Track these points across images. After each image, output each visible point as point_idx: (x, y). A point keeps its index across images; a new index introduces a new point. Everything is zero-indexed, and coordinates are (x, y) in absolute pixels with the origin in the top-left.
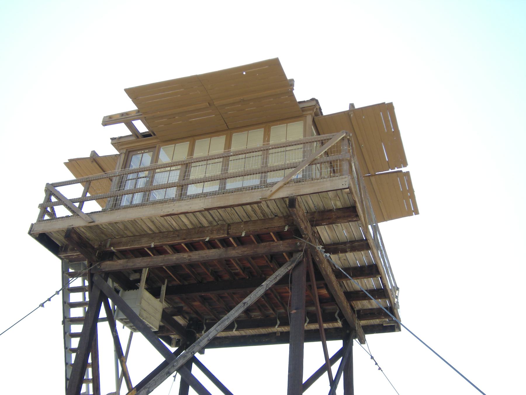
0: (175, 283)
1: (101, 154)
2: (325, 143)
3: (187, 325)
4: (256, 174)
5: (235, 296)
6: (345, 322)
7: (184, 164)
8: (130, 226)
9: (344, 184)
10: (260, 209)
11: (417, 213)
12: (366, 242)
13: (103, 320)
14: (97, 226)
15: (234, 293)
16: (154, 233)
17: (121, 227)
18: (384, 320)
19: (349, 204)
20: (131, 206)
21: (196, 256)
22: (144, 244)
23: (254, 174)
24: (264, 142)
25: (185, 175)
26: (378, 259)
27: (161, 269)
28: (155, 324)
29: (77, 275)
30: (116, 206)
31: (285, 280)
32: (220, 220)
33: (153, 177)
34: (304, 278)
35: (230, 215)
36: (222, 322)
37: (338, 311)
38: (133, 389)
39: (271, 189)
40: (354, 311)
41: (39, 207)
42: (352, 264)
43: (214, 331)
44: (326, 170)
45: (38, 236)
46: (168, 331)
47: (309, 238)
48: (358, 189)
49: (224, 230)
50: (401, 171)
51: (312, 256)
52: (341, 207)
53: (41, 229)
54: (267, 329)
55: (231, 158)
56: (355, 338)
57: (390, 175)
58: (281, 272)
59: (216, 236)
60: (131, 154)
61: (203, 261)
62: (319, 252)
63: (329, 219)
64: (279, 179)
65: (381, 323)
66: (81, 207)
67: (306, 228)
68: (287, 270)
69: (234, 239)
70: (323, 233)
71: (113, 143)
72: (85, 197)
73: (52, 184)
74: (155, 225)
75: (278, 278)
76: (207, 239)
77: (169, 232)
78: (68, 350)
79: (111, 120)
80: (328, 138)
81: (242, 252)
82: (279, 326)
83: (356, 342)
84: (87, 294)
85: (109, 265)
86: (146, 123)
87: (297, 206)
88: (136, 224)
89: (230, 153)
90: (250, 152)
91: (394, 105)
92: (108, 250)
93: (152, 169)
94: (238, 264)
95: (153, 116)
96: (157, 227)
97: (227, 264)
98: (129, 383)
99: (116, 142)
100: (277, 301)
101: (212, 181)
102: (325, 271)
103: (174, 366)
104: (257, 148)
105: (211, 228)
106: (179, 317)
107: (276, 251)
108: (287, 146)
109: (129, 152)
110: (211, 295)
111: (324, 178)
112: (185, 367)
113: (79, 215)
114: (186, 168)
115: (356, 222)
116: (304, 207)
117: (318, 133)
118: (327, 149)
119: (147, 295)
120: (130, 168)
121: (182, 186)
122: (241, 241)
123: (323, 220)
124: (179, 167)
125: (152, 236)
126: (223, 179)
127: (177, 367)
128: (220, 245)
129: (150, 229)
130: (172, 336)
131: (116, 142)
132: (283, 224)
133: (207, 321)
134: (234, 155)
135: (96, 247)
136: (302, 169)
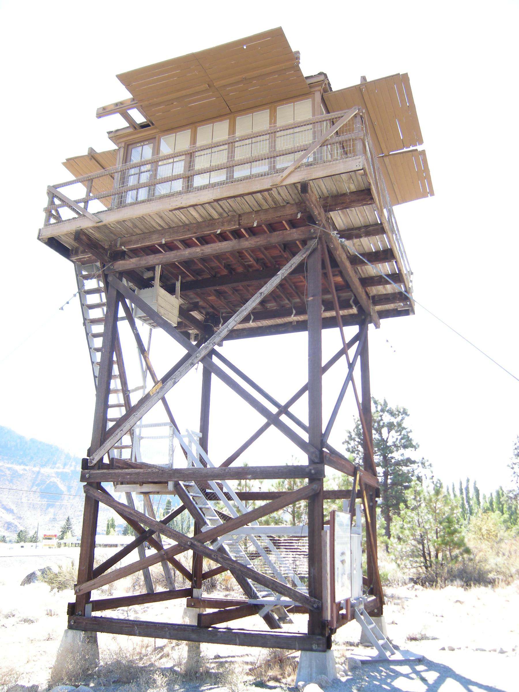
0: (188, 279)
1: (99, 149)
2: (337, 121)
3: (204, 320)
4: (265, 159)
5: (250, 288)
6: (361, 309)
7: (188, 154)
8: (138, 224)
9: (358, 165)
10: (270, 197)
11: (432, 193)
12: (381, 226)
13: (123, 319)
14: (105, 225)
15: (248, 286)
16: (164, 229)
17: (130, 224)
18: (398, 304)
19: (363, 187)
20: (137, 203)
21: (209, 249)
22: (155, 240)
23: (262, 160)
24: (270, 124)
25: (190, 165)
26: (393, 242)
27: (173, 265)
28: (173, 319)
29: (92, 276)
30: (121, 204)
31: (301, 268)
32: (230, 211)
33: (156, 170)
34: (320, 266)
35: (240, 205)
36: (240, 313)
37: (353, 298)
38: (158, 382)
39: (281, 174)
40: (369, 297)
41: (44, 211)
42: (367, 250)
43: (233, 323)
44: (338, 151)
45: (47, 240)
46: (186, 326)
47: (323, 224)
48: (372, 170)
49: (235, 221)
50: (416, 150)
51: (326, 243)
52: (355, 190)
53: (49, 233)
54: (283, 319)
55: (237, 144)
56: (371, 322)
57: (404, 154)
58: (296, 261)
59: (228, 228)
60: (130, 147)
61: (216, 254)
62: (333, 238)
63: (343, 203)
64: (289, 164)
65: (396, 308)
66: (86, 208)
67: (319, 214)
68: (302, 258)
69: (245, 229)
70: (336, 219)
71: (110, 137)
72: (89, 197)
73: (54, 186)
74: (164, 221)
75: (293, 267)
76: (219, 232)
77: (179, 227)
78: (92, 350)
79: (105, 111)
80: (339, 116)
81: (255, 242)
82: (295, 315)
83: (371, 327)
84: (103, 294)
85: (122, 265)
86: (143, 110)
87: (310, 191)
88: (144, 221)
89: (236, 139)
90: (257, 136)
91: (409, 76)
92: (119, 249)
93: (155, 162)
94: (251, 256)
95: (150, 104)
96: (166, 223)
97: (240, 256)
98: (154, 376)
99: (114, 136)
100: (292, 291)
101: (219, 169)
102: (340, 257)
103: (197, 357)
104: (264, 131)
105: (221, 220)
106: (195, 312)
107: (290, 240)
108: (296, 127)
109: (128, 145)
110: (226, 288)
111: (337, 160)
112: (207, 358)
113: (85, 216)
114: (191, 158)
115: (371, 205)
116: (316, 193)
117: (328, 112)
118: (338, 128)
119: (163, 292)
120: (131, 163)
121: (189, 177)
122: (252, 232)
123: (336, 205)
124: (183, 157)
125: (162, 232)
126: (230, 168)
127: (200, 358)
128: (231, 237)
129: (160, 225)
130: (190, 332)
131: (113, 136)
132: (296, 211)
133: (224, 315)
134: (240, 141)
135: (106, 247)
136: (313, 152)
